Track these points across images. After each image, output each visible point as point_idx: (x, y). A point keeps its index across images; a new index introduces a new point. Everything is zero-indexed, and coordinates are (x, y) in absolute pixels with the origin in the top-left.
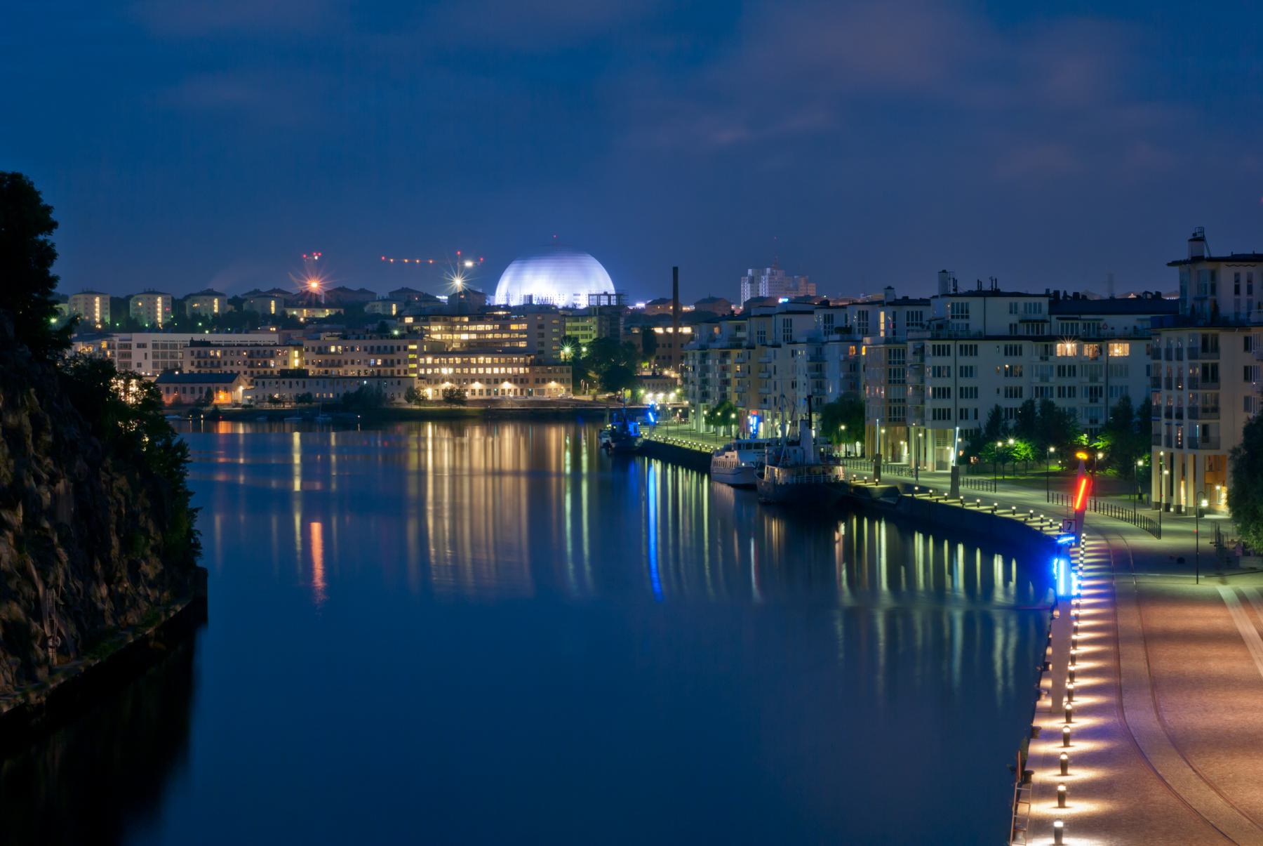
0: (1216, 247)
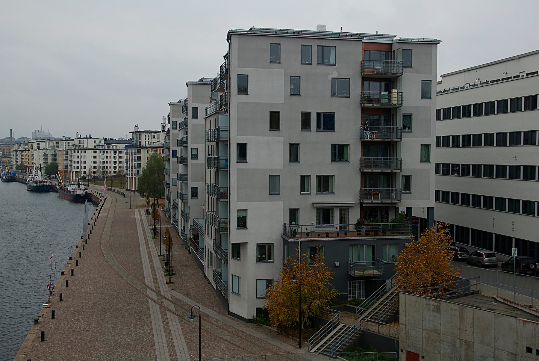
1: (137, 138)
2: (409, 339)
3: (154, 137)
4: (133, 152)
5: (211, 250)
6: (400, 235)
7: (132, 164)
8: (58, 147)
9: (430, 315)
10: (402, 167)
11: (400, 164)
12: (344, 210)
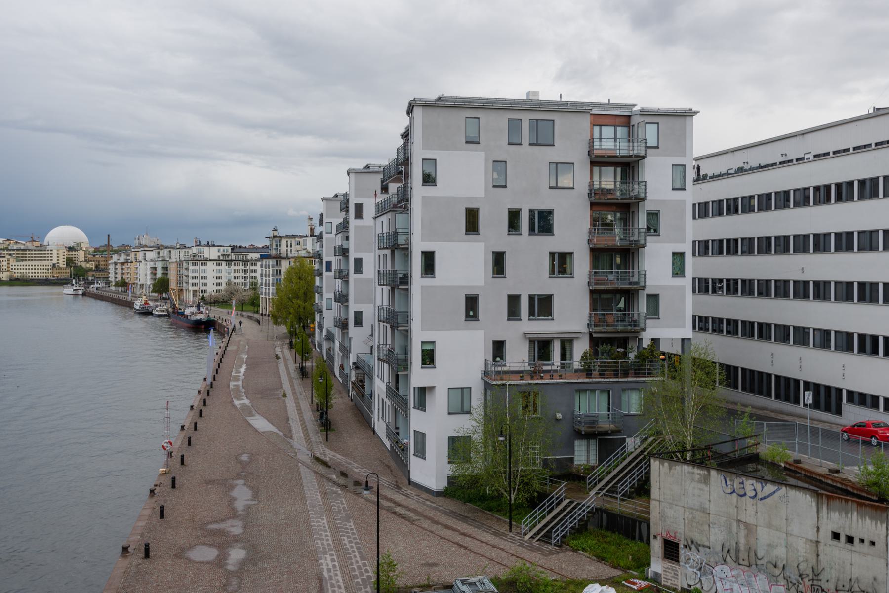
0: (281, 233)
1: (276, 246)
2: (665, 521)
3: (298, 244)
4: (271, 264)
5: (383, 396)
6: (645, 377)
7: (269, 280)
8: (170, 258)
9: (694, 488)
10: (647, 284)
11: (643, 280)
12: (567, 343)
